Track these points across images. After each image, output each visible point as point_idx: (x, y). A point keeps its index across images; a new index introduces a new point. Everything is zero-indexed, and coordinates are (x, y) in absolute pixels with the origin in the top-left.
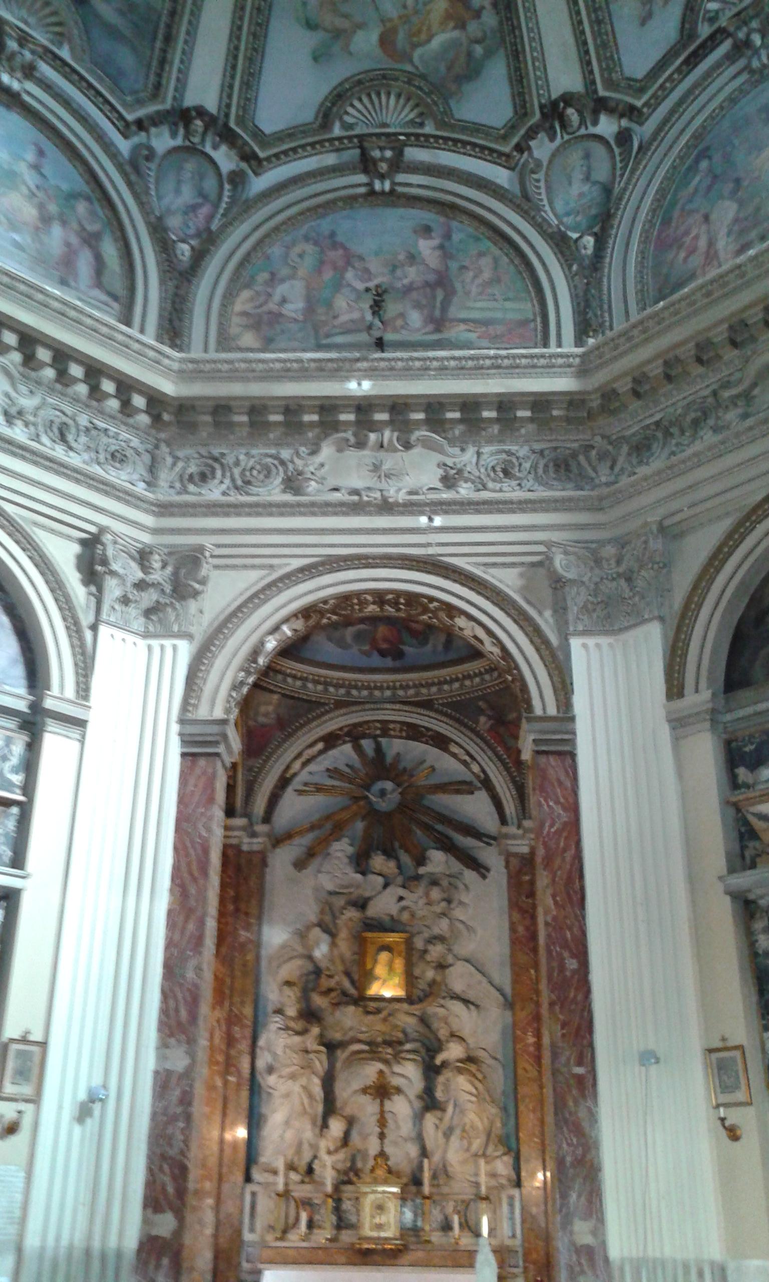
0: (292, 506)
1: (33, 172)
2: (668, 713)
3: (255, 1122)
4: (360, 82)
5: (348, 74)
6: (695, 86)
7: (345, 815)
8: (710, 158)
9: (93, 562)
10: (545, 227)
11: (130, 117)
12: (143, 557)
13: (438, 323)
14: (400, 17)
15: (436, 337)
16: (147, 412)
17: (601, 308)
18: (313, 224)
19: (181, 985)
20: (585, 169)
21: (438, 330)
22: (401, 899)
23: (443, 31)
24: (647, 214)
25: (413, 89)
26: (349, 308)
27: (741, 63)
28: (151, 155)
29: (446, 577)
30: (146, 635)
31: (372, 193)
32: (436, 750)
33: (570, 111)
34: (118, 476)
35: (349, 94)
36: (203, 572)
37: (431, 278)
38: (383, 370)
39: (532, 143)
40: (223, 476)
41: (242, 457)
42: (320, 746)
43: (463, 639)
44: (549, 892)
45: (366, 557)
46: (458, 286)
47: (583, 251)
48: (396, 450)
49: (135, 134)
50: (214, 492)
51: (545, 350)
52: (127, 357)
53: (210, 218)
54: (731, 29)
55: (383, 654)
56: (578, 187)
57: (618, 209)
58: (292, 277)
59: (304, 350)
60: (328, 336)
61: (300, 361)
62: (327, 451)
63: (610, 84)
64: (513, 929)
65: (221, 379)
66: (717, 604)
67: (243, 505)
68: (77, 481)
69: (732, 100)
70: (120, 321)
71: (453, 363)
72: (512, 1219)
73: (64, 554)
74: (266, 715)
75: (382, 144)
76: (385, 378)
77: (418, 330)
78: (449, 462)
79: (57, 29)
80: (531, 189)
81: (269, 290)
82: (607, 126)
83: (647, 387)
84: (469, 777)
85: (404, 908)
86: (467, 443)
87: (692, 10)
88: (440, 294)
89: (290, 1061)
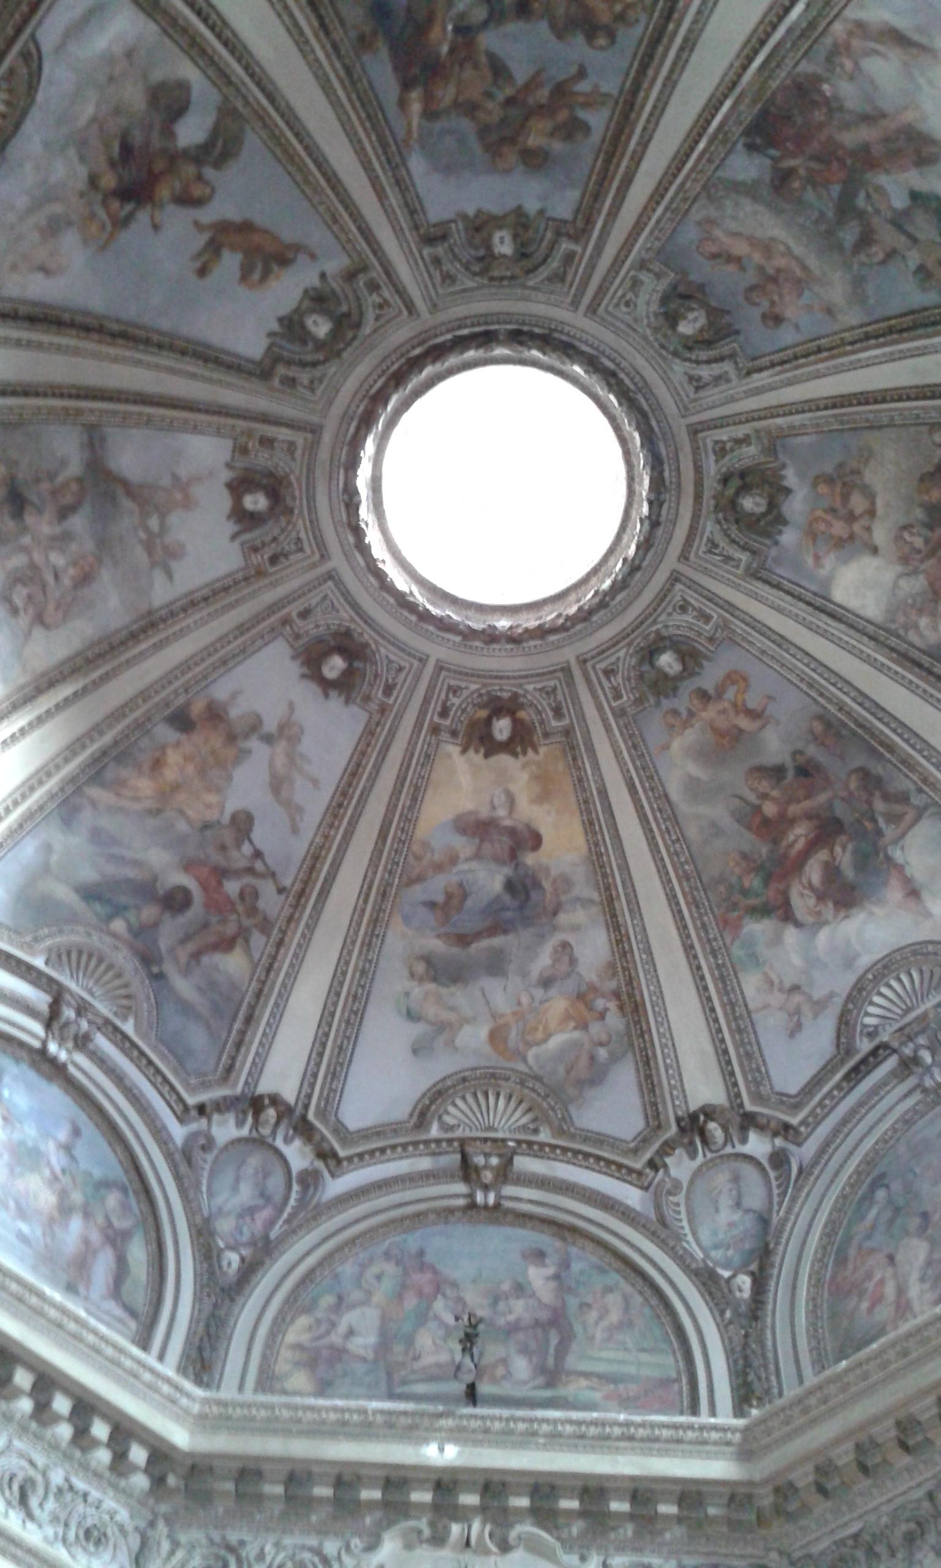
1: (62, 1153)
4: (464, 1080)
5: (449, 1071)
6: (861, 1104)
8: (887, 1187)
10: (688, 1261)
11: (191, 1100)
14: (514, 1014)
15: (548, 1393)
16: (146, 1471)
17: (766, 1366)
18: (398, 1239)
20: (734, 1193)
23: (562, 1031)
24: (816, 1251)
25: (526, 1091)
26: (434, 1347)
27: (912, 1081)
28: (208, 1144)
31: (472, 1206)
33: (712, 1125)
35: (451, 1091)
37: (544, 1315)
38: (474, 1431)
39: (668, 1160)
41: (269, 1548)
46: (578, 1329)
47: (738, 1294)
48: (487, 1552)
49: (195, 1120)
52: (134, 1392)
53: (271, 1223)
54: (895, 1044)
56: (726, 1215)
57: (777, 1244)
58: (365, 1302)
59: (371, 1398)
60: (404, 1382)
61: (363, 1412)
62: (390, 1546)
63: (758, 1098)
65: (253, 1431)
69: (907, 1121)
70: (133, 1342)
75: (487, 1150)
76: (477, 1443)
77: (525, 1383)
79: (125, 1002)
80: (669, 1213)
81: (333, 1317)
82: (757, 1145)
83: (837, 1481)
86: (588, 1548)
87: (847, 1023)
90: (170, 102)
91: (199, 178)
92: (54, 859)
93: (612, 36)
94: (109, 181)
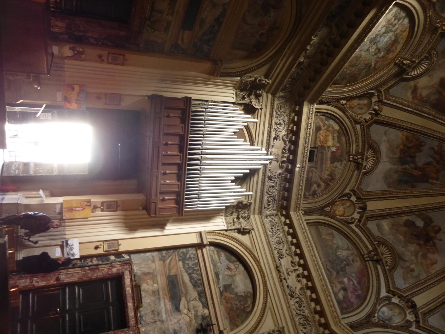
90: (410, 224)
91: (433, 227)
92: (221, 289)
93: (422, 142)
94: (422, 242)
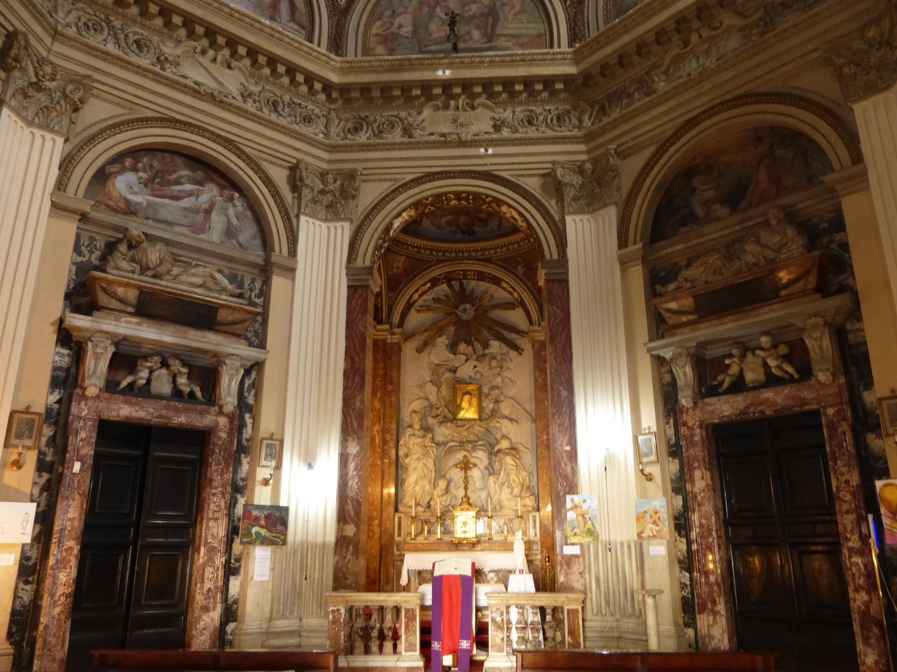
0: (406, 144)
2: (619, 256)
3: (399, 484)
7: (444, 323)
9: (296, 183)
12: (323, 175)
13: (490, 37)
17: (583, 26)
19: (353, 410)
21: (489, 41)
22: (475, 367)
26: (437, 29)
29: (496, 183)
30: (326, 220)
32: (495, 287)
34: (306, 130)
36: (357, 184)
37: (486, 11)
40: (368, 128)
42: (429, 285)
43: (507, 219)
44: (553, 356)
45: (449, 172)
50: (362, 138)
51: (551, 50)
52: (310, 61)
55: (463, 232)
58: (405, 12)
60: (426, 46)
61: (409, 59)
62: (427, 112)
64: (536, 381)
66: (647, 194)
67: (379, 145)
68: (285, 134)
71: (497, 59)
72: (535, 527)
73: (280, 176)
74: (398, 268)
76: (458, 68)
78: (497, 117)
84: (513, 300)
85: (477, 372)
88: (490, 21)
89: (417, 452)
